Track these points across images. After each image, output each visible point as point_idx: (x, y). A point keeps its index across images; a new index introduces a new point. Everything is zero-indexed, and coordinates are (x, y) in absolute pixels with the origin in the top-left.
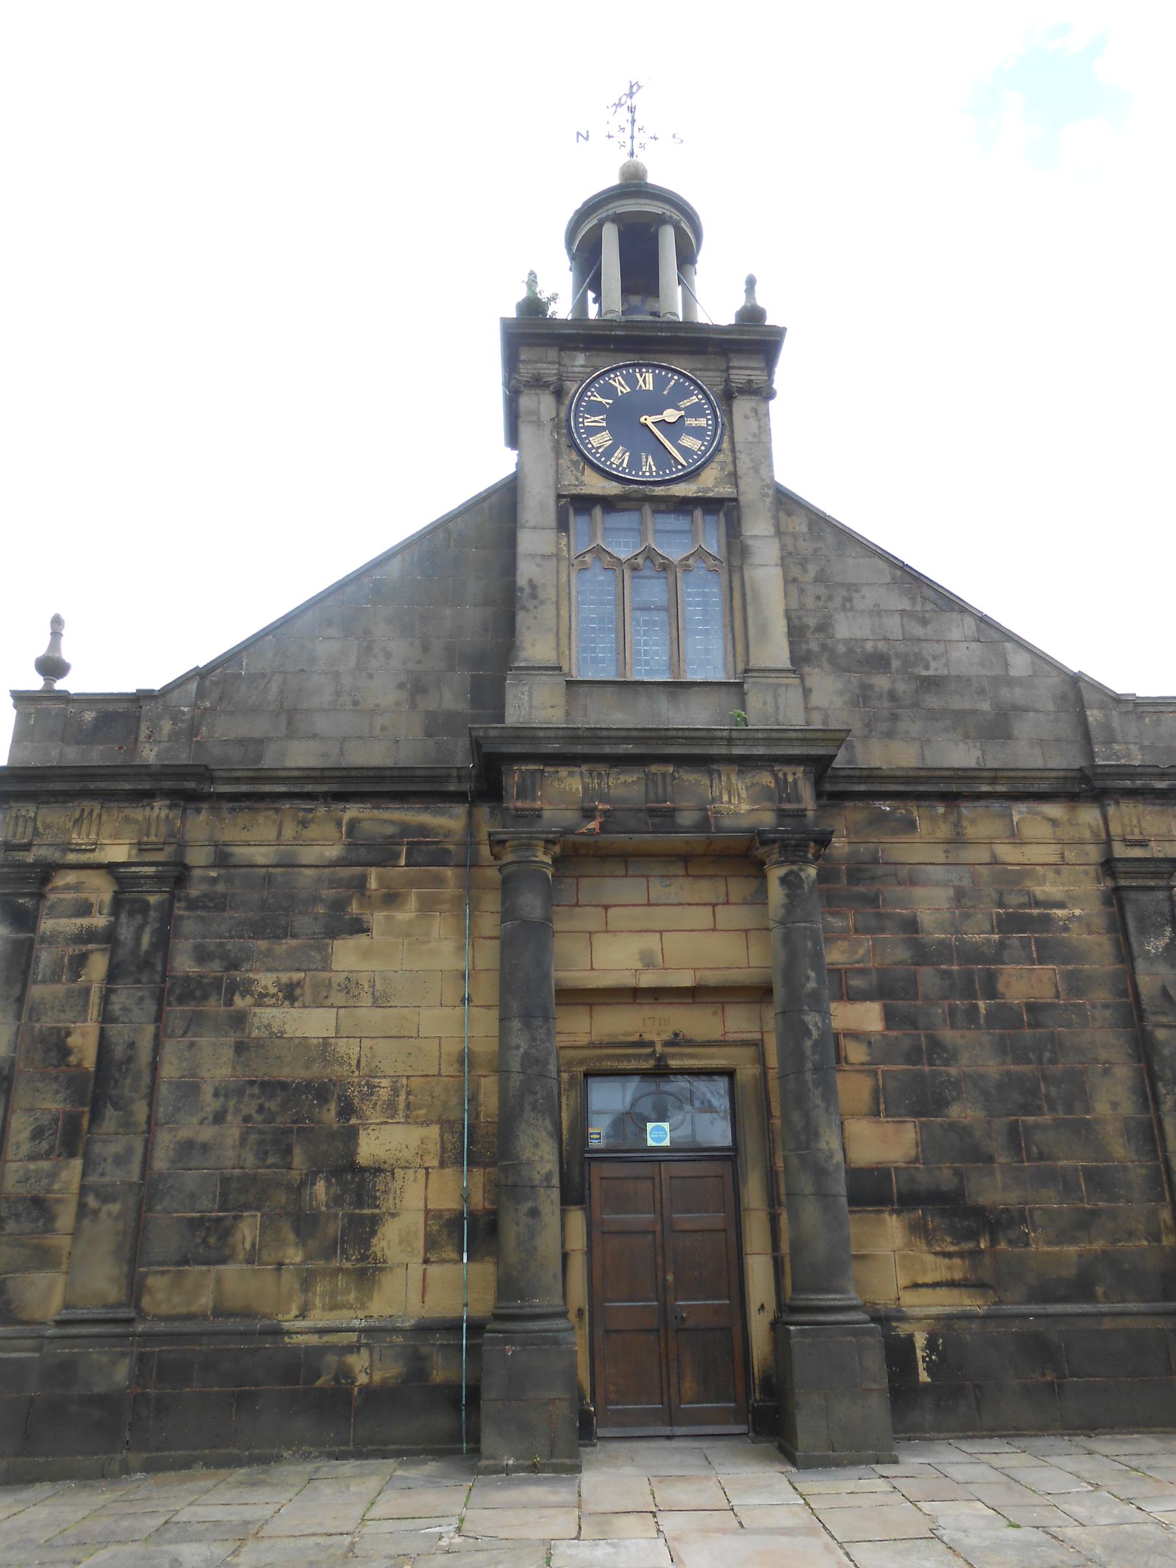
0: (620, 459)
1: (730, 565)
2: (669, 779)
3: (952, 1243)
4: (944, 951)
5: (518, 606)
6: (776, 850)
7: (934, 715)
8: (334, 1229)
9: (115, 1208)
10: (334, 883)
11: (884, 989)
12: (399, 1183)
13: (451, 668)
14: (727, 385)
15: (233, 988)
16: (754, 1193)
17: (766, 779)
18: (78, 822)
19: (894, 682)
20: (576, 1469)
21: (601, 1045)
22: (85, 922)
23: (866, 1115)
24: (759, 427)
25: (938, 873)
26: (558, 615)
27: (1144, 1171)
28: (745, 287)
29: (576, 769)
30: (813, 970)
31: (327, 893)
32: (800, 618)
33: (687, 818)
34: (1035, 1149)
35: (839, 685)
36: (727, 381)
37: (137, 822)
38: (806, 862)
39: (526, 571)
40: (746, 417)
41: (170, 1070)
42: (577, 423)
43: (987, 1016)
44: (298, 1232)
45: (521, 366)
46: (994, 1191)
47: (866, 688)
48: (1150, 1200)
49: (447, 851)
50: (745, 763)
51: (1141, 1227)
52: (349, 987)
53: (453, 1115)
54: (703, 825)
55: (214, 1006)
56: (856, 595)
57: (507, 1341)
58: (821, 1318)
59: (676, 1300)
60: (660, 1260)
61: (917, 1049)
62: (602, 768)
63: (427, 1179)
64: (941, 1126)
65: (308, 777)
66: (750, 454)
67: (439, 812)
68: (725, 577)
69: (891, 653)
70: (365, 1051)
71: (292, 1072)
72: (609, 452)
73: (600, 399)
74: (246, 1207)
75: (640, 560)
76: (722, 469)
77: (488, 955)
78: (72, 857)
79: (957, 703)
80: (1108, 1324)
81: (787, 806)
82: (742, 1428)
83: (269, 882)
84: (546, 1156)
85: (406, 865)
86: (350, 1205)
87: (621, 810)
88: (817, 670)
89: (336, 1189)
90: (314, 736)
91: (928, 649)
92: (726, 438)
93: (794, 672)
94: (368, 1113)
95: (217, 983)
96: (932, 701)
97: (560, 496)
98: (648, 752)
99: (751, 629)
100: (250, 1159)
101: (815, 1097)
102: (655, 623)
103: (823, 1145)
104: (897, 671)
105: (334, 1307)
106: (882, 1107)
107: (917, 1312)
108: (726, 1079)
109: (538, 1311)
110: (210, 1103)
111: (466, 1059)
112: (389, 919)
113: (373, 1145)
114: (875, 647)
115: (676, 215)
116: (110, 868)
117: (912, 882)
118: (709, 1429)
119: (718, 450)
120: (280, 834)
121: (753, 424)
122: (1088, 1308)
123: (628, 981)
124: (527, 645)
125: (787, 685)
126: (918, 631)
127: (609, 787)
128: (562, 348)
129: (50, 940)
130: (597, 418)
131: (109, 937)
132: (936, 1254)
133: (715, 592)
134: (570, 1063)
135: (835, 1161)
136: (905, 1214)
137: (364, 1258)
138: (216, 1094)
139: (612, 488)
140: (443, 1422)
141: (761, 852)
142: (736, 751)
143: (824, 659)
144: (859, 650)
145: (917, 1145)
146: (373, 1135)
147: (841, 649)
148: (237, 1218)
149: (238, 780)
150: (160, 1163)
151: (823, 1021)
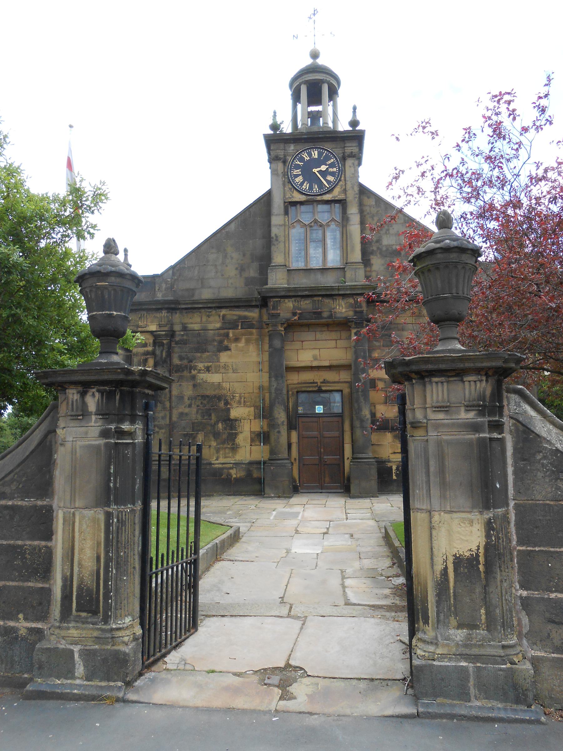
1: (343, 224)
8: (225, 436)
9: (163, 431)
10: (220, 335)
12: (242, 424)
13: (253, 262)
15: (191, 368)
16: (347, 427)
17: (351, 301)
21: (301, 383)
22: (146, 349)
25: (410, 326)
26: (285, 246)
31: (217, 338)
33: (325, 315)
35: (383, 262)
36: (344, 153)
37: (158, 317)
39: (274, 231)
40: (350, 167)
44: (214, 438)
49: (253, 324)
50: (344, 296)
52: (225, 367)
53: (258, 404)
54: (330, 316)
55: (186, 373)
58: (359, 461)
62: (299, 299)
67: (250, 311)
70: (231, 386)
71: (210, 392)
72: (302, 184)
74: (199, 430)
76: (341, 188)
77: (266, 357)
81: (358, 309)
82: (343, 491)
89: (224, 426)
90: (210, 287)
95: (186, 367)
97: (285, 202)
98: (312, 294)
99: (349, 248)
100: (199, 417)
103: (363, 413)
105: (226, 457)
107: (394, 460)
110: (187, 402)
111: (261, 388)
112: (236, 346)
115: (329, 78)
116: (152, 332)
117: (403, 330)
118: (335, 491)
119: (340, 180)
121: (352, 169)
123: (309, 364)
124: (275, 258)
125: (359, 268)
128: (285, 143)
129: (137, 354)
131: (153, 353)
134: (292, 389)
137: (233, 444)
138: (189, 399)
139: (302, 198)
140: (257, 487)
142: (340, 293)
144: (390, 249)
146: (235, 410)
147: (384, 249)
148: (197, 434)
149: (187, 304)
150: (174, 419)
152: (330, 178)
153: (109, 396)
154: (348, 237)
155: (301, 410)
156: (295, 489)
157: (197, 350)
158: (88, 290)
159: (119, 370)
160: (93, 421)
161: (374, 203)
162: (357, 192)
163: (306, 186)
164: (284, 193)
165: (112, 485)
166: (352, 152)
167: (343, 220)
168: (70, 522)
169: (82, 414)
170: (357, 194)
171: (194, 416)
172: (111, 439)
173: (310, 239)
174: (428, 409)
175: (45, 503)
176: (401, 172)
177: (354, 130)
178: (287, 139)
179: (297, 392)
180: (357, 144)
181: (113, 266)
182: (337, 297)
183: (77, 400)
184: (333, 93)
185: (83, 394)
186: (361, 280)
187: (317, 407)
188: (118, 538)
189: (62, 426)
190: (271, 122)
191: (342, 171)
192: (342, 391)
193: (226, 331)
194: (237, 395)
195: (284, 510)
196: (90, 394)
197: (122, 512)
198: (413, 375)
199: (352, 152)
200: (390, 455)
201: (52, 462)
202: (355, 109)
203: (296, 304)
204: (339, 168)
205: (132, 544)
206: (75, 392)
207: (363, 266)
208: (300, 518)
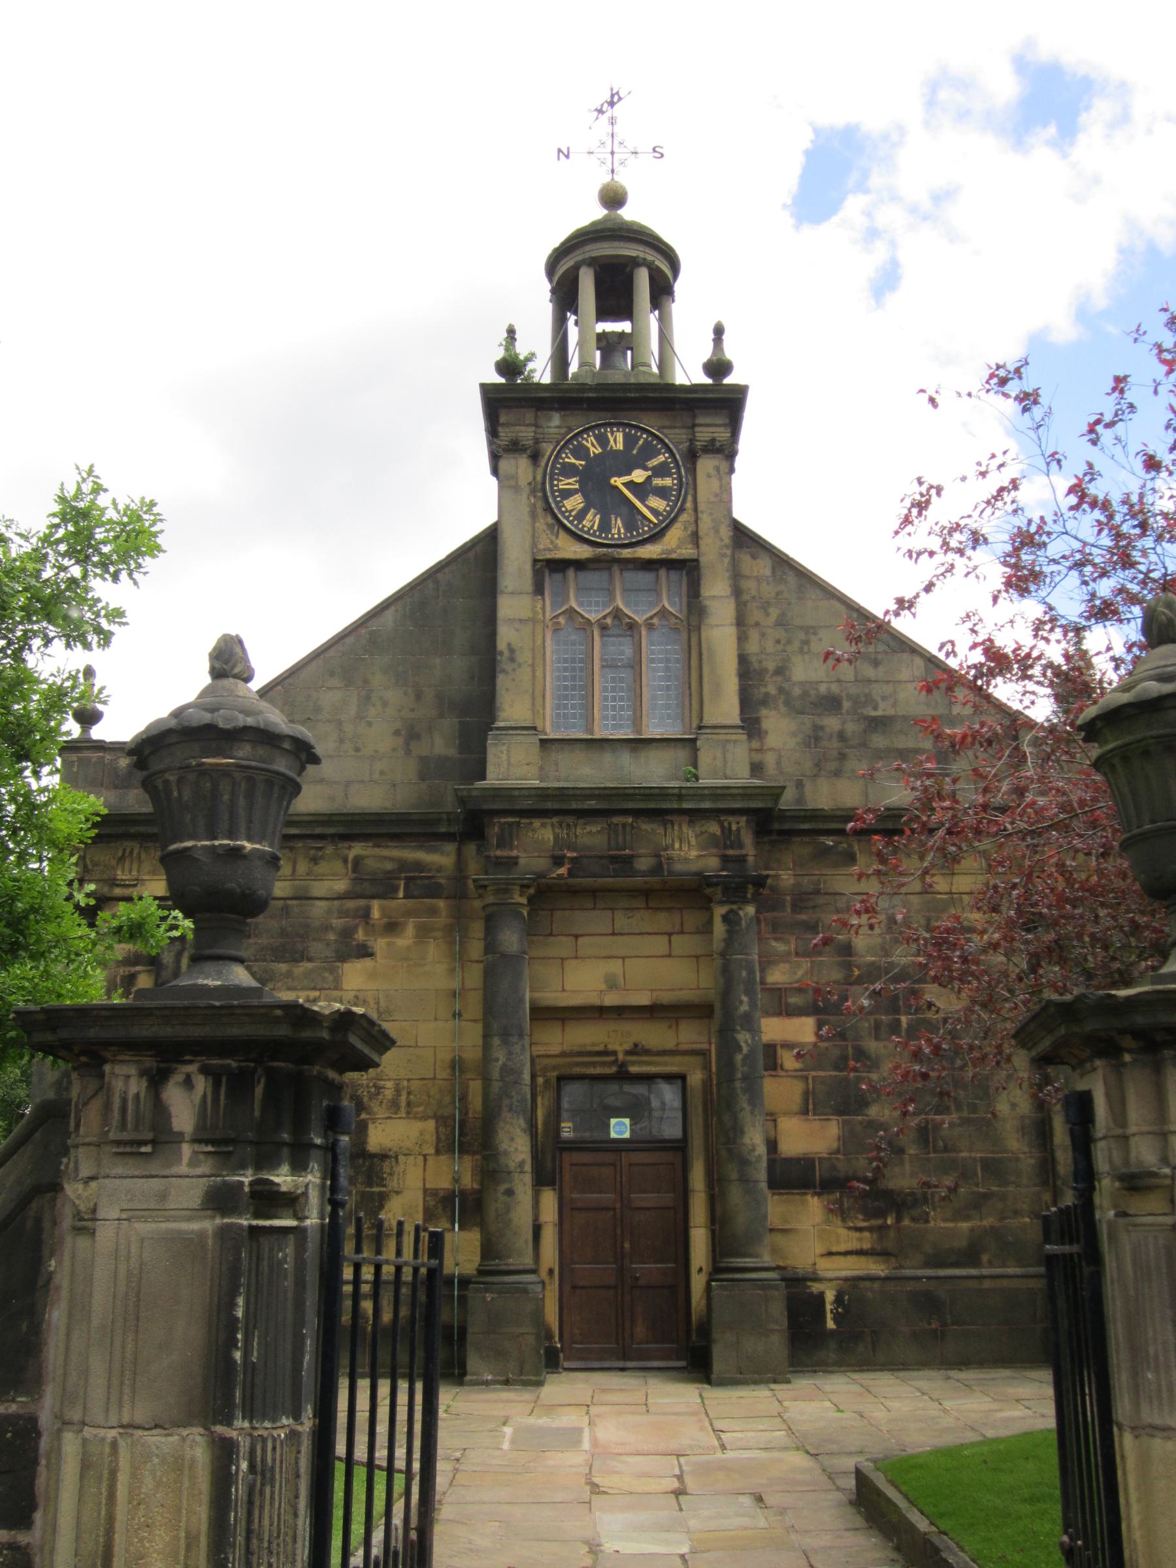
2: (628, 829)
3: (863, 1220)
4: (872, 973)
5: (498, 669)
6: (719, 892)
7: (879, 755)
11: (820, 1007)
13: (441, 716)
14: (691, 444)
17: (714, 828)
18: (121, 859)
19: (844, 723)
20: (539, 1384)
21: (571, 1054)
23: (796, 1114)
24: (721, 487)
26: (534, 676)
27: (1033, 1161)
28: (712, 336)
29: (549, 821)
30: (746, 995)
31: (337, 923)
32: (760, 662)
33: (643, 864)
34: (941, 1143)
36: (692, 441)
38: (746, 902)
39: (506, 635)
42: (552, 486)
43: (907, 1030)
45: (500, 429)
46: (903, 1179)
47: (817, 728)
48: (1035, 1185)
49: (440, 885)
50: (694, 815)
51: (1025, 1207)
54: (657, 870)
56: (813, 638)
57: (487, 1291)
58: (731, 1276)
59: (632, 1263)
60: (619, 1232)
61: (845, 1058)
62: (570, 820)
63: (425, 1165)
64: (861, 1123)
65: (316, 822)
66: (711, 514)
68: (685, 635)
69: (843, 695)
72: (581, 515)
73: (573, 461)
75: (609, 621)
76: (685, 529)
77: (474, 977)
78: (118, 891)
79: (902, 742)
80: (987, 1284)
81: (730, 852)
82: (682, 1364)
83: (287, 913)
84: (520, 1148)
85: (405, 898)
86: (362, 1184)
87: (587, 857)
88: (773, 713)
90: (322, 781)
91: (877, 690)
92: (690, 498)
93: (742, 728)
94: (375, 1110)
96: (879, 741)
97: (535, 561)
101: (743, 1102)
102: (622, 680)
103: (747, 1140)
104: (848, 713)
106: (811, 1107)
107: (830, 1274)
108: (679, 1082)
109: (512, 1268)
111: (457, 1065)
112: (389, 944)
113: (379, 1136)
114: (829, 689)
115: (651, 256)
118: (656, 1364)
119: (682, 509)
120: (294, 870)
121: (715, 484)
122: (973, 1272)
123: (594, 1000)
124: (506, 706)
125: (735, 741)
126: (870, 672)
127: (576, 836)
130: (570, 481)
132: (849, 1228)
133: (674, 650)
134: (545, 1069)
135: (756, 1153)
136: (825, 1197)
139: (582, 552)
141: (708, 891)
142: (686, 805)
143: (780, 701)
144: (813, 692)
145: (839, 1139)
146: (380, 1127)
147: (797, 691)
151: (753, 1039)
152: (657, 503)
153: (233, 1086)
154: (705, 657)
155: (567, 1130)
156: (552, 1361)
158: (172, 778)
159: (278, 1012)
160: (185, 1159)
161: (768, 572)
162: (727, 541)
163: (592, 520)
164: (533, 536)
165: (238, 1355)
166: (713, 440)
167: (689, 611)
168: (98, 1471)
169: (151, 1139)
170: (726, 546)
172: (240, 1215)
173: (602, 660)
174: (1133, 1141)
175: (13, 1408)
176: (933, 492)
177: (718, 386)
178: (542, 400)
179: (560, 1079)
180: (727, 421)
181: (247, 713)
182: (675, 818)
183: (137, 1096)
184: (662, 291)
185: (157, 1080)
186: (739, 776)
187: (613, 1121)
188: (249, 1521)
189: (85, 1172)
190: (500, 354)
191: (688, 486)
192: (682, 1078)
193: (362, 902)
195: (532, 1420)
196: (179, 1077)
197: (264, 1440)
198: (1128, 1042)
199: (713, 440)
201: (40, 1283)
202: (719, 331)
203: (563, 834)
204: (680, 478)
205: (289, 1539)
206: (132, 1070)
207: (745, 737)
208: (586, 1445)
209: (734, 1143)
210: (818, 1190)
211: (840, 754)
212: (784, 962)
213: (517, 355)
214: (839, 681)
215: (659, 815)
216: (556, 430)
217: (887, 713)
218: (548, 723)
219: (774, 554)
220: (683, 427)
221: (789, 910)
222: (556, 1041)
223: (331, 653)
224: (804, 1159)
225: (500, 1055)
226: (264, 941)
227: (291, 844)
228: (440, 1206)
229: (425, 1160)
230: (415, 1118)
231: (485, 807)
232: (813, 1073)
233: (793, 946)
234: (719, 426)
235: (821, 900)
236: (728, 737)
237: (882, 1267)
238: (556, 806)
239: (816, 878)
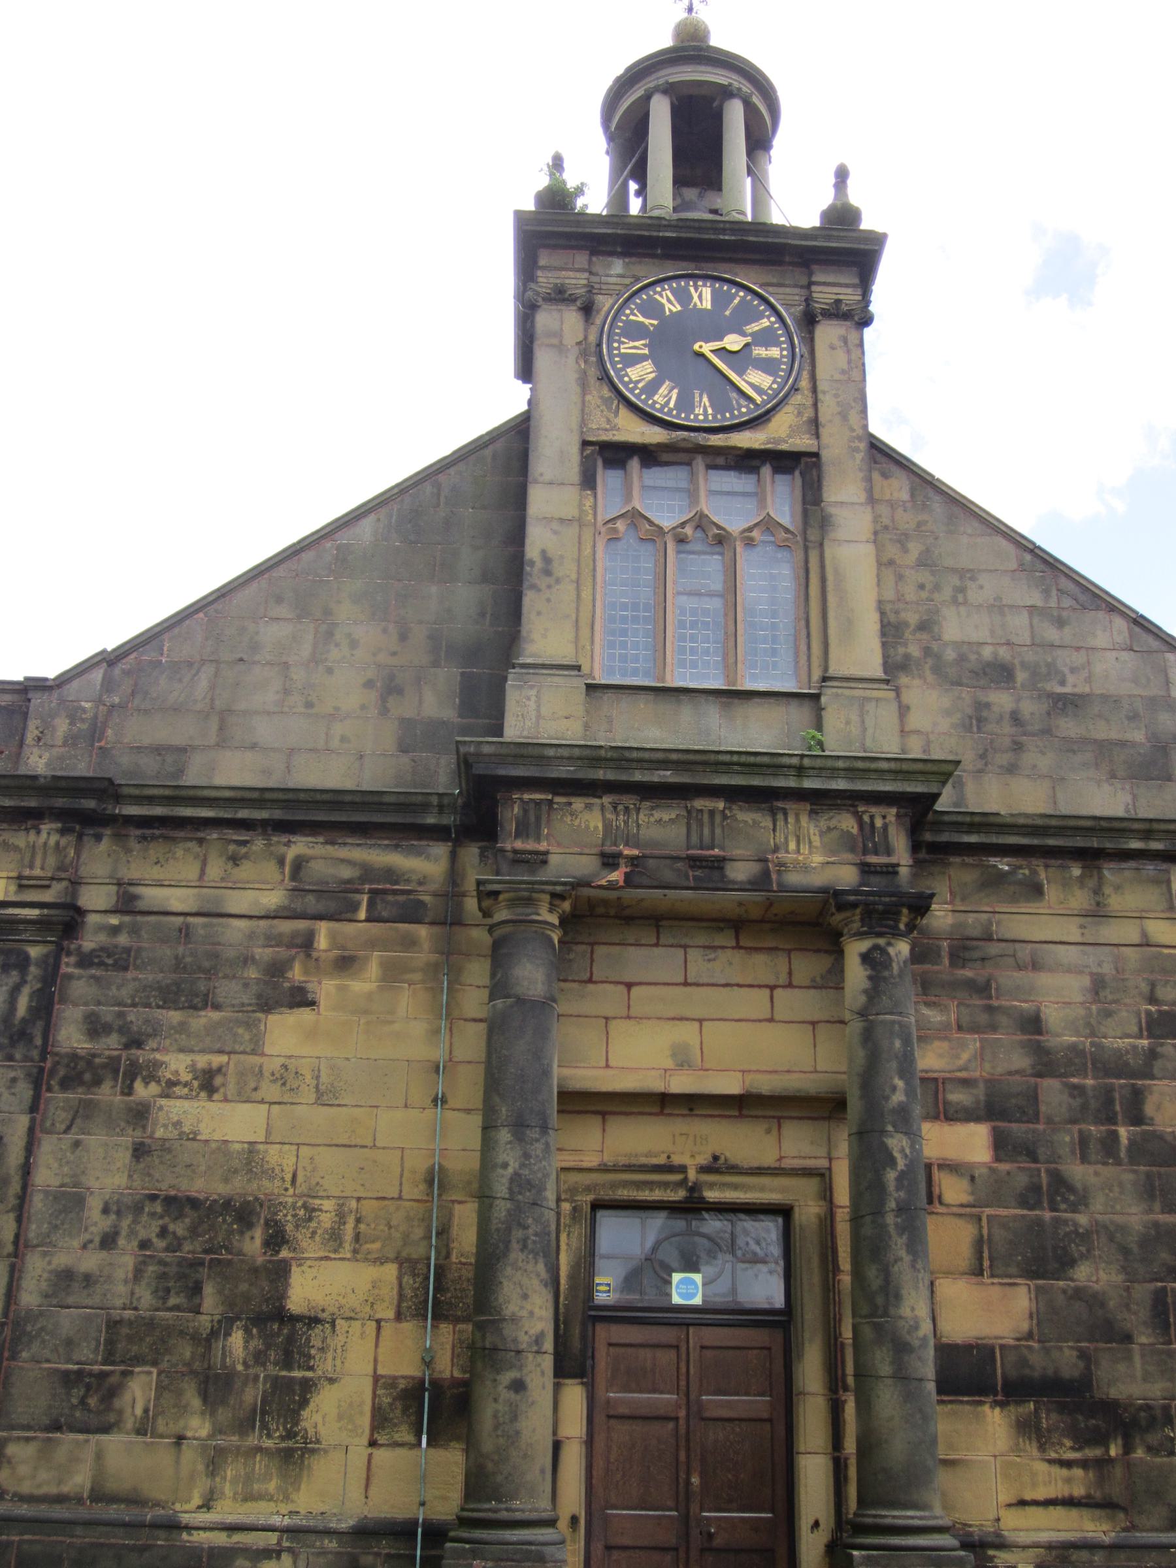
0: (665, 399)
1: (806, 540)
2: (718, 818)
3: (1072, 1448)
4: (1076, 1060)
6: (857, 918)
7: (1071, 746)
8: (252, 1395)
10: (272, 940)
11: (995, 1108)
12: (341, 1339)
13: (436, 664)
14: (808, 305)
15: (133, 1072)
17: (847, 823)
19: (1018, 700)
28: (833, 180)
30: (901, 1078)
31: (263, 953)
32: (897, 612)
33: (740, 872)
36: (808, 300)
37: (16, 849)
38: (897, 934)
39: (537, 540)
40: (833, 348)
41: (46, 1176)
44: (205, 1396)
47: (981, 707)
49: (421, 903)
50: (820, 801)
53: (417, 1252)
54: (761, 881)
55: (108, 1094)
59: (702, 1509)
61: (1036, 1188)
62: (629, 800)
64: (1064, 1291)
65: (242, 800)
66: (836, 396)
68: (800, 555)
69: (1016, 662)
72: (652, 388)
73: (641, 319)
74: (139, 1360)
75: (688, 530)
76: (800, 414)
77: (470, 1043)
79: (1102, 731)
81: (873, 859)
83: (187, 935)
85: (367, 920)
89: (256, 1343)
90: (253, 746)
91: (1065, 659)
92: (805, 374)
94: (304, 1244)
95: (113, 1065)
96: (1068, 727)
97: (585, 443)
100: (146, 1298)
103: (905, 1311)
105: (249, 1497)
106: (986, 1263)
107: (1023, 1538)
109: (518, 1516)
110: (97, 1222)
111: (436, 1180)
112: (342, 989)
113: (305, 1289)
114: (995, 654)
115: (747, 88)
117: (1035, 965)
120: (203, 872)
123: (656, 1084)
124: (535, 636)
125: (877, 700)
126: (1051, 634)
128: (594, 252)
130: (637, 344)
132: (1051, 1462)
134: (573, 1191)
135: (921, 1333)
136: (1012, 1408)
137: (290, 1435)
138: (106, 1211)
141: (837, 919)
142: (808, 784)
143: (927, 666)
144: (973, 657)
146: (310, 1273)
147: (950, 655)
149: (151, 800)
150: (29, 1298)
151: (912, 1147)
152: (763, 380)
157: (170, 997)
161: (905, 495)
166: (838, 302)
171: (121, 1289)
179: (596, 1206)
180: (856, 281)
182: (789, 806)
193: (301, 925)
194: (328, 1205)
200: (1003, 1513)
202: (842, 175)
209: (886, 1314)
210: (999, 1398)
211: (1015, 743)
212: (939, 1039)
213: (564, 182)
214: (1008, 643)
215: (765, 798)
216: (618, 280)
217: (1078, 690)
218: (596, 666)
219: (913, 472)
220: (796, 286)
221: (946, 961)
222: (590, 1146)
223: (280, 572)
224: (978, 1346)
225: (509, 1156)
226: (148, 976)
227: (200, 835)
228: (399, 1404)
229: (379, 1328)
230: (366, 1260)
231: (502, 772)
232: (989, 1211)
233: (953, 1017)
234: (847, 286)
235: (993, 949)
236: (868, 693)
237: (1105, 1527)
238: (611, 775)
239: (985, 916)
